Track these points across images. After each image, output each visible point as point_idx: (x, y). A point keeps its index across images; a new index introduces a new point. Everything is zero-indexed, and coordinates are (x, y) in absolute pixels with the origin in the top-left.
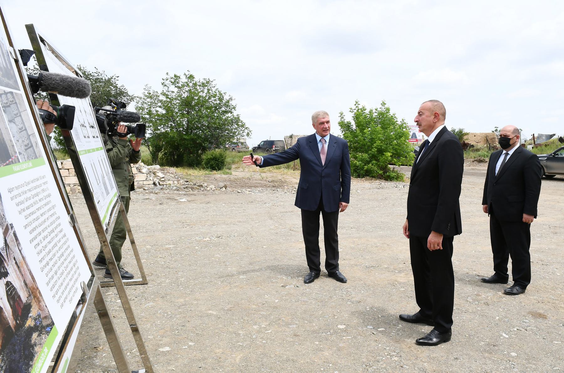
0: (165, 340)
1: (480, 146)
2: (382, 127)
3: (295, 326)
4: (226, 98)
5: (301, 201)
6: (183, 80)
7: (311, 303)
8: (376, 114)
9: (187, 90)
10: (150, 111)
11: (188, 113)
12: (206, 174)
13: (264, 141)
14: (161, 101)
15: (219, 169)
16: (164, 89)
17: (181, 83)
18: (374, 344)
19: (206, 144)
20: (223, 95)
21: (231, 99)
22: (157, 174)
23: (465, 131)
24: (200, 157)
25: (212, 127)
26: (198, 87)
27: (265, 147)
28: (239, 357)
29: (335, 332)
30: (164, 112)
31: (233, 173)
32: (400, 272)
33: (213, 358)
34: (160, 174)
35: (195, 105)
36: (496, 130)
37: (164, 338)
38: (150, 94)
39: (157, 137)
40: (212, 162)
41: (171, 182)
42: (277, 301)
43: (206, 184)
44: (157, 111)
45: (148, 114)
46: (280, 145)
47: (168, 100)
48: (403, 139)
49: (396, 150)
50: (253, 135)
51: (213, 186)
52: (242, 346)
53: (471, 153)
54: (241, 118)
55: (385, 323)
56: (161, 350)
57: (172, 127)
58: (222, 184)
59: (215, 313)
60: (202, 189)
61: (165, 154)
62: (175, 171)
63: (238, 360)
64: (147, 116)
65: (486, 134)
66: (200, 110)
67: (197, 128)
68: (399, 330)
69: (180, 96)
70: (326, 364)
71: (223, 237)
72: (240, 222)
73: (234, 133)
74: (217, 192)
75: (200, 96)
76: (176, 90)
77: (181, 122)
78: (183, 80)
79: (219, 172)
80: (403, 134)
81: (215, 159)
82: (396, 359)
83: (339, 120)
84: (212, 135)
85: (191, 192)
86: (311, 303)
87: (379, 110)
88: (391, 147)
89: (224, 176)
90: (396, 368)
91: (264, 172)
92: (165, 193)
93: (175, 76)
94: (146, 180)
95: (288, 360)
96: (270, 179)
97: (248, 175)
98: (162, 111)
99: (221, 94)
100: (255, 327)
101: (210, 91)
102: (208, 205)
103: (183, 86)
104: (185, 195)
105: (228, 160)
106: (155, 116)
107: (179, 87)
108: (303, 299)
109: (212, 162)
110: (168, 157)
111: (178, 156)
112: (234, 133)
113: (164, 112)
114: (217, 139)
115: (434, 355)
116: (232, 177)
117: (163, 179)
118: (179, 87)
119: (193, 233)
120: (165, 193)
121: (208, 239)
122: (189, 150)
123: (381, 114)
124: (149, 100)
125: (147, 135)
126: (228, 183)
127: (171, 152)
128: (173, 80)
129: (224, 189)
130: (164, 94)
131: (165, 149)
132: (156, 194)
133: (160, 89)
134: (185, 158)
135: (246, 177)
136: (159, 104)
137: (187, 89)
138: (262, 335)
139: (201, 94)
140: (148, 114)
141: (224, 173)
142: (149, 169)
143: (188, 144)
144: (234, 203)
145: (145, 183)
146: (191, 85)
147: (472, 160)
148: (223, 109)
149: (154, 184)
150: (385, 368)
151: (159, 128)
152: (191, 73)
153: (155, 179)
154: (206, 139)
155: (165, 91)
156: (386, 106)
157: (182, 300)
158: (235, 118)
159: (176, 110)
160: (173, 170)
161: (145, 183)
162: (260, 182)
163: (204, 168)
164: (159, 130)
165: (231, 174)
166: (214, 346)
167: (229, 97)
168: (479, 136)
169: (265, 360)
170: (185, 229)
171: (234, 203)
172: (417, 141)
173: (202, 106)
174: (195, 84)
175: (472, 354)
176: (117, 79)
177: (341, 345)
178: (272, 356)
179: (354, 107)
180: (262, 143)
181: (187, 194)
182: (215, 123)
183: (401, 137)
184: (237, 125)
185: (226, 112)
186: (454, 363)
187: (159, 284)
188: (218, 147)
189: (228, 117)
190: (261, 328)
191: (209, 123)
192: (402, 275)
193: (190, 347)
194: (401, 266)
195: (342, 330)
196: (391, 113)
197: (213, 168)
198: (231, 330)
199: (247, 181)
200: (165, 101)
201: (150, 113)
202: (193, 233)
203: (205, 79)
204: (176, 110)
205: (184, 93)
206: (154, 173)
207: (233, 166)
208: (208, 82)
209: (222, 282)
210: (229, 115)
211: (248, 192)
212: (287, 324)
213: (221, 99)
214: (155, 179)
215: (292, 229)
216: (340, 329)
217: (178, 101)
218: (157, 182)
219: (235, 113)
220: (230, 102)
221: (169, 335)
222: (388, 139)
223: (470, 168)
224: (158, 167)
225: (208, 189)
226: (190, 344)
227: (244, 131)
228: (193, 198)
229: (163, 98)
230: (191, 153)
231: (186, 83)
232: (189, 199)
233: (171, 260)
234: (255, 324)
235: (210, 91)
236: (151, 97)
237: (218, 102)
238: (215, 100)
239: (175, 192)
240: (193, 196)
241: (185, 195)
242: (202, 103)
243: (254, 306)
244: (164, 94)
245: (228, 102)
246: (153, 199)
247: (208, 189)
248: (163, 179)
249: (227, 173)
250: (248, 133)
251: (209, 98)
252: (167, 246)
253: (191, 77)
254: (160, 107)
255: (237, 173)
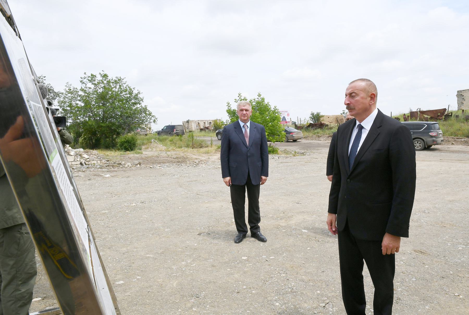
0: (119, 277)
1: (332, 125)
2: (260, 113)
3: (211, 260)
4: (135, 92)
5: (227, 170)
6: (99, 78)
7: (221, 244)
8: (255, 103)
9: (102, 86)
10: (71, 104)
11: (104, 105)
12: (121, 154)
13: (167, 126)
14: (80, 96)
15: (132, 150)
16: (82, 86)
17: (97, 81)
18: (268, 267)
19: (120, 130)
20: (133, 90)
21: (139, 93)
22: (83, 156)
23: (322, 114)
24: (115, 140)
25: (125, 116)
26: (111, 84)
27: (168, 130)
28: (175, 283)
29: (241, 262)
30: (83, 105)
31: (144, 152)
32: (281, 219)
33: (157, 285)
34: (86, 156)
35: (109, 99)
36: (344, 113)
37: (117, 276)
38: (71, 90)
39: (76, 125)
40: (126, 145)
41: (95, 162)
42: (196, 245)
43: (123, 163)
44: (77, 104)
45: (69, 106)
46: (179, 128)
47: (86, 94)
48: (276, 121)
49: (271, 130)
50: (158, 122)
51: (129, 164)
52: (176, 276)
53: (327, 131)
54: (148, 108)
55: (274, 253)
56: (117, 283)
57: (90, 117)
58: (137, 162)
59: (152, 256)
60: (121, 166)
61: (85, 139)
62: (97, 153)
63: (175, 285)
64: (69, 108)
65: (336, 116)
66: (113, 103)
67: (111, 117)
68: (284, 257)
69: (96, 91)
70: (237, 282)
71: (146, 203)
72: (157, 190)
73: (143, 121)
74: (133, 168)
75: (113, 91)
76: (93, 86)
77: (97, 112)
78: (99, 78)
79: (132, 152)
80: (276, 117)
81: (128, 141)
82: (284, 275)
83: (226, 108)
84: (125, 123)
85: (113, 169)
86: (221, 244)
87: (257, 100)
88: (267, 128)
89: (136, 155)
90: (284, 281)
91: (169, 151)
92: (91, 171)
93: (92, 75)
94: (74, 161)
95: (210, 282)
96: (175, 156)
97: (156, 154)
98: (81, 104)
99: (131, 89)
100: (183, 263)
101: (122, 87)
102: (129, 179)
103: (99, 83)
104: (107, 171)
105: (139, 142)
106: (75, 108)
107: (95, 84)
108: (214, 242)
109: (126, 145)
110: (87, 141)
111: (96, 140)
112: (143, 121)
113: (83, 105)
114: (129, 126)
115: (309, 271)
116: (143, 156)
117: (88, 160)
118: (95, 84)
119: (121, 200)
120: (91, 171)
121: (134, 204)
122: (106, 135)
123: (258, 103)
124: (69, 95)
125: (68, 124)
126: (141, 161)
127: (90, 137)
128: (90, 79)
129: (139, 165)
130: (82, 90)
131: (84, 135)
132: (84, 172)
133: (79, 86)
134: (102, 141)
135: (155, 155)
136: (79, 98)
137: (103, 85)
138: (189, 268)
139: (114, 89)
140: (69, 106)
141: (136, 153)
142: (76, 152)
143: (104, 131)
144: (150, 177)
145: (73, 163)
146: (105, 82)
147: (327, 136)
148: (133, 101)
149: (81, 164)
150: (277, 281)
151: (79, 118)
152: (105, 73)
153: (82, 160)
154: (120, 126)
155: (83, 88)
156: (261, 97)
157: (125, 249)
158: (144, 108)
159: (93, 103)
160: (95, 152)
161: (73, 163)
162: (166, 159)
163: (119, 150)
164: (79, 119)
165: (142, 153)
166: (156, 277)
167: (138, 92)
168: (332, 117)
169: (194, 283)
170: (114, 198)
171: (150, 177)
172: (286, 122)
173: (115, 99)
174: (109, 82)
175: (333, 268)
176: (44, 78)
177: (246, 270)
178: (199, 280)
179: (238, 98)
180: (165, 128)
181: (109, 171)
182: (127, 113)
183: (274, 120)
184: (146, 114)
185: (135, 104)
186: (322, 274)
187: (105, 239)
188: (129, 132)
189: (137, 108)
190: (187, 263)
191: (122, 112)
192: (283, 221)
193: (138, 279)
194: (282, 215)
195: (245, 260)
196: (266, 102)
197: (126, 149)
198: (166, 266)
199: (156, 159)
200: (83, 96)
201: (70, 106)
202: (121, 200)
203: (117, 77)
204: (93, 103)
205: (100, 89)
206: (80, 155)
207: (143, 147)
208: (119, 80)
209: (153, 234)
210: (138, 106)
211: (158, 168)
212: (206, 259)
213: (131, 93)
214: (82, 160)
215: (198, 193)
216: (244, 260)
217: (94, 96)
218: (83, 163)
219: (143, 104)
220: (139, 96)
221: (121, 273)
222: (265, 121)
223: (326, 142)
224: (82, 150)
225: (126, 166)
226: (138, 277)
227: (151, 119)
228: (115, 173)
229: (81, 93)
230: (107, 137)
231: (102, 80)
232: (112, 174)
233: (109, 222)
234: (183, 261)
235: (122, 87)
236: (72, 93)
237: (129, 95)
238: (126, 94)
239: (99, 170)
240: (115, 173)
241: (107, 171)
242: (115, 97)
243: (180, 249)
244: (82, 90)
245: (137, 95)
246: (82, 176)
247: (126, 166)
248: (88, 160)
249: (139, 153)
250: (154, 120)
251: (121, 93)
252: (103, 212)
253: (105, 76)
254: (80, 101)
255: (147, 153)
